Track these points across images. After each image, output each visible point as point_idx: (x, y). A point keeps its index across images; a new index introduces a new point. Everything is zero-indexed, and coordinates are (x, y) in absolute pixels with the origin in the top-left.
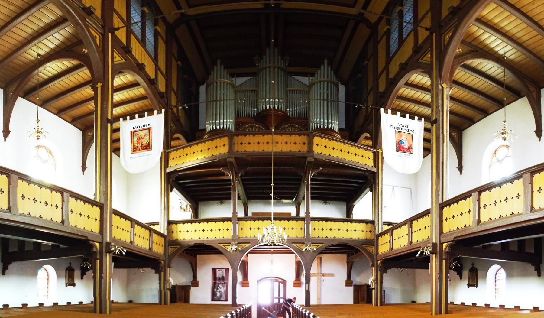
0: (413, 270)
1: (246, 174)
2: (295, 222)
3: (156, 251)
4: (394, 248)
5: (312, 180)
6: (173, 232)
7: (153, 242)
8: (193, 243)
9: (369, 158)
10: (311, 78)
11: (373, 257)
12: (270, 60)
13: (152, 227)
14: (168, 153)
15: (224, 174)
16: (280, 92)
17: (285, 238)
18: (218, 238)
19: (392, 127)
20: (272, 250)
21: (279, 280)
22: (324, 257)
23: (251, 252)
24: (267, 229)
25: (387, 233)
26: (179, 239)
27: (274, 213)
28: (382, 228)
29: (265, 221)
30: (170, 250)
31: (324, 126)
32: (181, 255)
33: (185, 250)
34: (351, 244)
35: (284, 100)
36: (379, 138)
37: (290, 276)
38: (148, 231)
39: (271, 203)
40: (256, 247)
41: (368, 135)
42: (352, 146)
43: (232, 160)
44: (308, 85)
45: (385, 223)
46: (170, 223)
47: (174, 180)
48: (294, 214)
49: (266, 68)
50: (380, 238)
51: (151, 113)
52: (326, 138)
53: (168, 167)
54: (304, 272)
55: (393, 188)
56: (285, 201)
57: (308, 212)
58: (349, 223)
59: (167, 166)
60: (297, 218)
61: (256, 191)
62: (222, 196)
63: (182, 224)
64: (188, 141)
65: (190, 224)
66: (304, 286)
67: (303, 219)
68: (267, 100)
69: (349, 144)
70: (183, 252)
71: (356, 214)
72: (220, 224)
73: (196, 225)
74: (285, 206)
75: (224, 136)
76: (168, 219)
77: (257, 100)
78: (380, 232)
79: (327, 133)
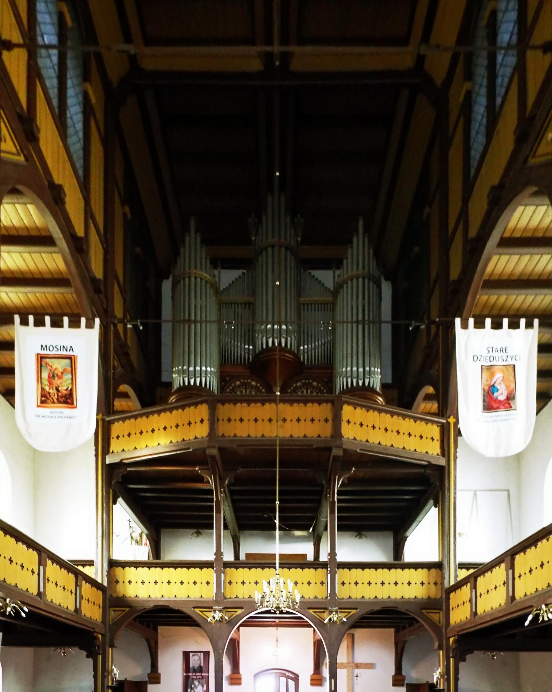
0: (515, 653)
1: (237, 481)
2: (312, 570)
3: (88, 615)
4: (480, 611)
5: (340, 493)
6: (117, 582)
7: (81, 598)
8: (152, 605)
9: (433, 439)
10: (338, 272)
11: (440, 630)
12: (273, 226)
13: (80, 568)
14: (110, 423)
15: (201, 480)
16: (288, 292)
17: (298, 600)
18: (192, 598)
19: (475, 358)
20: (277, 621)
21: (287, 674)
22: (359, 633)
23: (244, 625)
24: (269, 583)
25: (466, 584)
26: (128, 595)
27: (280, 555)
28: (456, 576)
29: (266, 570)
30: (113, 615)
31: (358, 383)
32: (131, 626)
33: (138, 617)
34: (402, 609)
35: (296, 328)
36: (451, 393)
37: (305, 667)
38: (72, 576)
39: (274, 537)
40: (252, 614)
41: (430, 390)
42: (404, 417)
43: (214, 452)
44: (332, 289)
45: (462, 566)
46: (113, 564)
47: (121, 482)
48: (310, 557)
49: (266, 249)
50: (452, 595)
51: (75, 324)
52: (362, 406)
53: (108, 452)
54: (327, 660)
55: (475, 494)
56: (298, 533)
57: (333, 554)
58: (399, 570)
59: (106, 450)
60: (316, 564)
61: (251, 519)
62: (200, 524)
63: (133, 569)
64: (144, 404)
65: (146, 569)
66: (327, 684)
67: (324, 565)
68: (269, 326)
69: (399, 415)
70: (135, 619)
71: (411, 553)
72: (195, 573)
73: (156, 572)
74: (296, 542)
75: (201, 403)
76: (109, 556)
77: (253, 325)
78: (452, 583)
79: (361, 395)
